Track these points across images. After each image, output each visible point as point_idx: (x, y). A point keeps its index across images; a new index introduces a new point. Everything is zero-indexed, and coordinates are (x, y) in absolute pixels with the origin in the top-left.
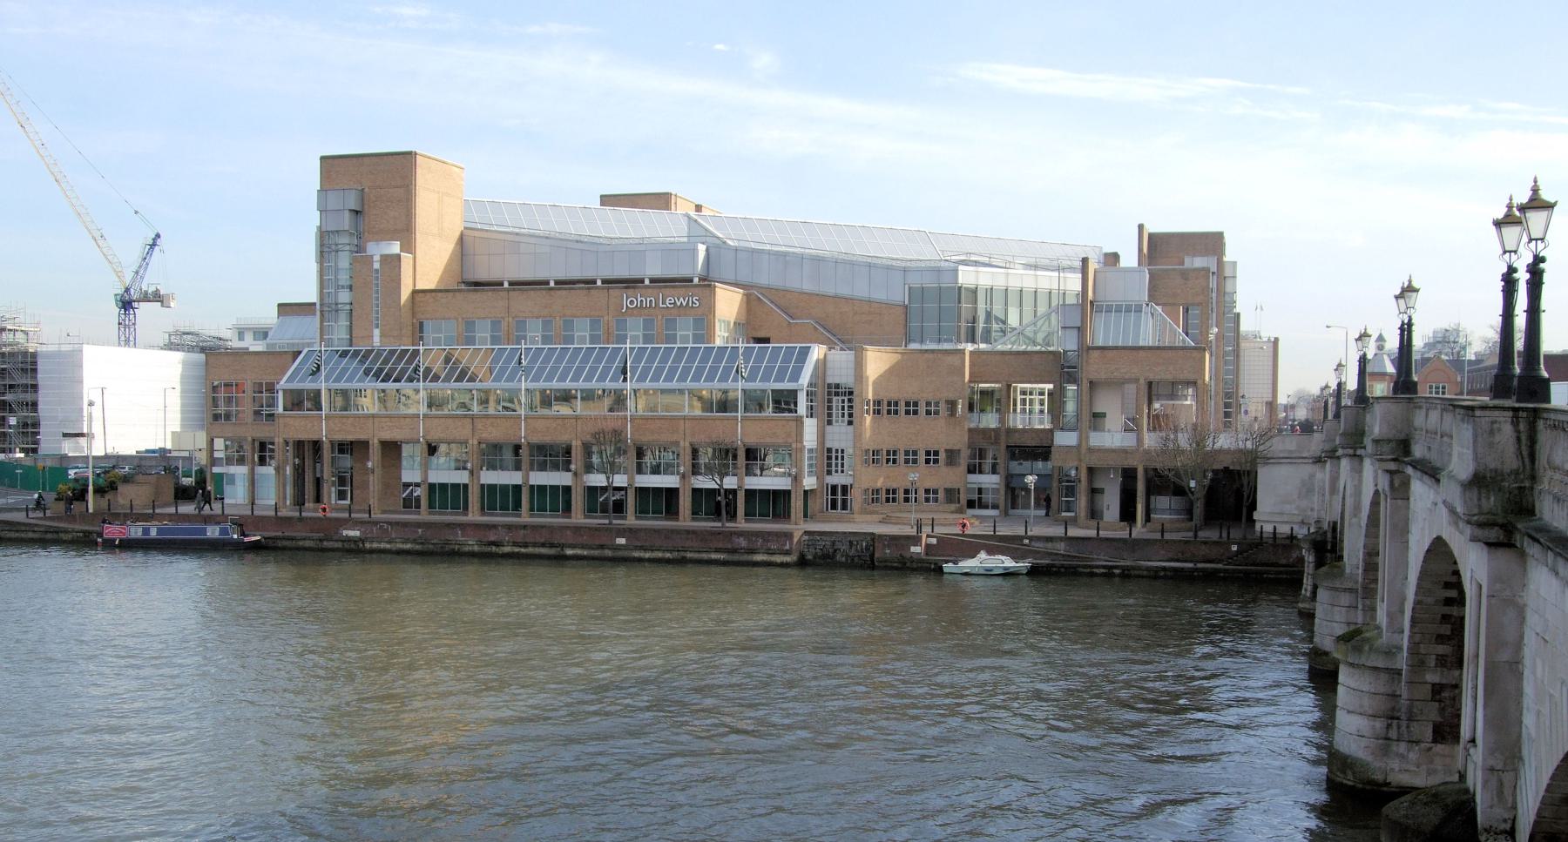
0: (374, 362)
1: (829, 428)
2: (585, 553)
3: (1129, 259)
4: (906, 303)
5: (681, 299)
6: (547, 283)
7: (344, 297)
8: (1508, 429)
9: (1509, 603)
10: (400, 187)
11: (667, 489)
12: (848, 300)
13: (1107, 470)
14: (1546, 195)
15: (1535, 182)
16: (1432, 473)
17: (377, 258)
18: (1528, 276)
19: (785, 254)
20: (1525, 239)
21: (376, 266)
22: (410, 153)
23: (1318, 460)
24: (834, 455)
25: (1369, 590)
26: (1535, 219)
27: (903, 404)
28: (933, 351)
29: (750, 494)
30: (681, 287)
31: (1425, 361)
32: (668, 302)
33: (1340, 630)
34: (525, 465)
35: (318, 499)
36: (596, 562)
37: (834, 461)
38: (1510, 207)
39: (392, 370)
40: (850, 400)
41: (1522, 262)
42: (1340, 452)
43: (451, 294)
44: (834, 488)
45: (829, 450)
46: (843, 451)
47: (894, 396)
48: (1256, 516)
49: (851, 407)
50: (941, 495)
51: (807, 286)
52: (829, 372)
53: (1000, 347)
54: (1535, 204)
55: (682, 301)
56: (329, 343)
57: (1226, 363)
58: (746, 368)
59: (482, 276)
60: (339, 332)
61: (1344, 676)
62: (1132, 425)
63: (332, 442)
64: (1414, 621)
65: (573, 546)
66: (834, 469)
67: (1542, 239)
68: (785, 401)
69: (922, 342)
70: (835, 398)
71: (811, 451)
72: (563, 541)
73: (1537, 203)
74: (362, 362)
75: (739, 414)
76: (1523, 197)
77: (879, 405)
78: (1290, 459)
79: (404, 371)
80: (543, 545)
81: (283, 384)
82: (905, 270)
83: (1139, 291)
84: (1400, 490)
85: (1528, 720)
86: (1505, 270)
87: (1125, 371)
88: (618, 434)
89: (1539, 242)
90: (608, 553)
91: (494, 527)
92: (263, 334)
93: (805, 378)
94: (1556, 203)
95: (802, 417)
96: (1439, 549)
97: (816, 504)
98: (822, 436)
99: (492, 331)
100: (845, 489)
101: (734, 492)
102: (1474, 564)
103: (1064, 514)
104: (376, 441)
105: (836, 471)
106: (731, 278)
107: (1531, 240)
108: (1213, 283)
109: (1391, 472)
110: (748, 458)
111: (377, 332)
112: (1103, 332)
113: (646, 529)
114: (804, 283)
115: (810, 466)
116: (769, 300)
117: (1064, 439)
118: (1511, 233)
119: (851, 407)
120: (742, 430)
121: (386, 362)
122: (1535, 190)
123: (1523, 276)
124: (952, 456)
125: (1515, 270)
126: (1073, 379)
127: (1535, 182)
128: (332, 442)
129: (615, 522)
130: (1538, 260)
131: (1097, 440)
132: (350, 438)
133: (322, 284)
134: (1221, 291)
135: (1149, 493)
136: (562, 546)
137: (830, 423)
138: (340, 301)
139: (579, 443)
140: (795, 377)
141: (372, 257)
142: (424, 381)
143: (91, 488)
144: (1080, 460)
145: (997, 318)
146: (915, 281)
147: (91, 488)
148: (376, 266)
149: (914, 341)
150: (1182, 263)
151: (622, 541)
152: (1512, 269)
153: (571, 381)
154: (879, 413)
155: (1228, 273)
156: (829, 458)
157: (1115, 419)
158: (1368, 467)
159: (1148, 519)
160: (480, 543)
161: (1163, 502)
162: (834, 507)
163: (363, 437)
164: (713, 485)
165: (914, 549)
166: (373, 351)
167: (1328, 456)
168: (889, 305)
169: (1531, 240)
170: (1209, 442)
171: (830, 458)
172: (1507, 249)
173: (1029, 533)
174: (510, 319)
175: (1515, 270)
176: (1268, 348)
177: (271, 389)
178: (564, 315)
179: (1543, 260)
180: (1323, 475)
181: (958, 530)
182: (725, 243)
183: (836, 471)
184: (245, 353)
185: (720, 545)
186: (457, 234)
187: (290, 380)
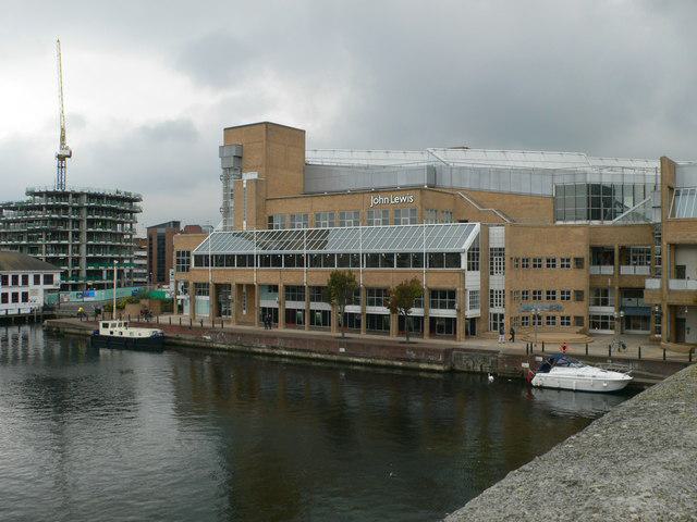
1: (491, 277)
12: (518, 195)
13: (683, 307)
29: (433, 319)
34: (616, 263)
39: (268, 244)
44: (495, 315)
45: (492, 291)
49: (551, 263)
52: (491, 241)
79: (268, 244)
80: (300, 350)
81: (194, 252)
90: (335, 358)
93: (467, 245)
100: (502, 316)
103: (559, 223)
114: (490, 185)
124: (579, 295)
132: (223, 282)
140: (462, 243)
144: (662, 298)
145: (619, 204)
146: (559, 181)
151: (342, 350)
160: (268, 347)
168: (543, 197)
171: (491, 296)
177: (188, 253)
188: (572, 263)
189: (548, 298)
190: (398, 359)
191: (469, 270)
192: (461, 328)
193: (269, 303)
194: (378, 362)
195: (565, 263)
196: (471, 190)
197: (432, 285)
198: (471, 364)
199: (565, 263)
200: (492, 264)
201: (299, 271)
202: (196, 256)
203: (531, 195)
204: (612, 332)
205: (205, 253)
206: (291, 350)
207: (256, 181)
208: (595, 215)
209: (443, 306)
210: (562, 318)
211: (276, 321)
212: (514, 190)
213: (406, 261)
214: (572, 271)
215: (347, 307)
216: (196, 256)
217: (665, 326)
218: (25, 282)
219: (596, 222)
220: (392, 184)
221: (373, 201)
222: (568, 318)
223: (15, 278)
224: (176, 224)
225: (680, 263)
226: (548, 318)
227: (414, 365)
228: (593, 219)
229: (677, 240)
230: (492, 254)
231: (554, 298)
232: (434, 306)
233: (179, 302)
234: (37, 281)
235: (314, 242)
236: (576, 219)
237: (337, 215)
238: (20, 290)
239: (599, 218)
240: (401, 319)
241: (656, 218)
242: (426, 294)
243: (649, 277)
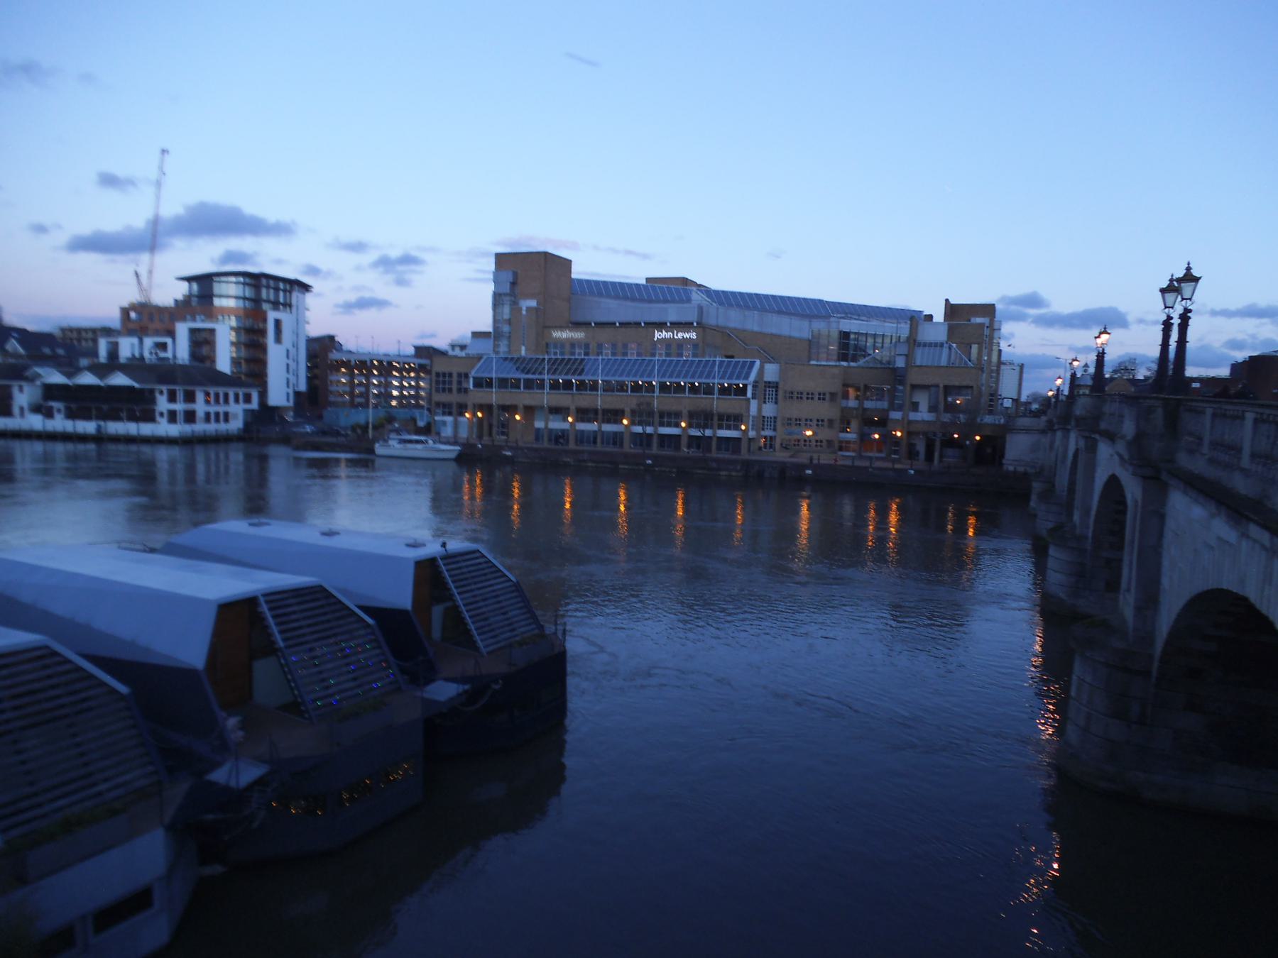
0: (521, 364)
1: (764, 405)
3: (939, 317)
4: (810, 338)
6: (615, 324)
7: (506, 329)
8: (1160, 411)
9: (1156, 515)
12: (779, 336)
13: (917, 434)
14: (1195, 273)
15: (1189, 264)
16: (1111, 437)
17: (524, 308)
18: (1179, 321)
20: (1179, 298)
21: (524, 312)
23: (1043, 432)
25: (1069, 507)
26: (1188, 289)
27: (805, 394)
28: (824, 365)
31: (1112, 379)
32: (679, 335)
33: (1050, 525)
35: (490, 434)
37: (766, 423)
38: (1171, 280)
40: (776, 391)
41: (1179, 309)
42: (1056, 427)
45: (764, 417)
47: (833, 390)
48: (1004, 461)
49: (810, 396)
51: (756, 329)
54: (1187, 278)
56: (497, 353)
57: (992, 377)
59: (581, 319)
60: (503, 348)
61: (1052, 551)
62: (933, 409)
64: (1096, 521)
67: (1190, 299)
69: (818, 360)
70: (768, 389)
71: (753, 417)
73: (1190, 278)
74: (515, 363)
75: (599, 393)
76: (1180, 273)
78: (1027, 430)
79: (537, 369)
81: (473, 373)
83: (941, 336)
84: (1092, 448)
85: (1165, 581)
86: (1165, 318)
89: (1188, 301)
91: (583, 452)
92: (463, 347)
94: (1200, 278)
95: (749, 399)
96: (1113, 484)
98: (760, 409)
101: (710, 438)
102: (1133, 490)
104: (521, 406)
107: (1183, 299)
108: (987, 332)
109: (1086, 438)
110: (719, 420)
111: (523, 348)
112: (921, 357)
115: (753, 425)
116: (735, 336)
118: (1170, 297)
119: (776, 395)
120: (719, 404)
121: (527, 364)
122: (1188, 269)
123: (1176, 321)
124: (831, 422)
125: (1172, 318)
126: (902, 383)
127: (1189, 264)
130: (1187, 311)
131: (913, 416)
133: (495, 321)
134: (991, 338)
135: (1164, 399)
140: (747, 377)
142: (548, 374)
143: (370, 426)
147: (370, 426)
148: (524, 312)
149: (814, 360)
150: (970, 321)
151: (649, 462)
152: (1169, 318)
156: (764, 421)
157: (924, 406)
158: (1073, 436)
159: (941, 461)
161: (950, 452)
163: (514, 403)
164: (699, 434)
167: (1049, 428)
168: (801, 340)
169: (1183, 299)
170: (979, 420)
172: (1167, 306)
173: (873, 466)
175: (1172, 318)
177: (467, 376)
179: (1190, 311)
180: (1045, 440)
181: (832, 462)
184: (456, 357)
188: (827, 397)
191: (753, 399)
195: (822, 397)
196: (735, 329)
197: (722, 410)
199: (822, 397)
200: (765, 395)
202: (474, 378)
203: (790, 337)
207: (536, 310)
214: (826, 404)
218: (226, 401)
219: (845, 364)
220: (662, 320)
223: (217, 395)
228: (843, 360)
230: (765, 386)
232: (662, 424)
234: (237, 400)
237: (620, 345)
238: (221, 409)
239: (846, 361)
241: (900, 363)
242: (716, 418)
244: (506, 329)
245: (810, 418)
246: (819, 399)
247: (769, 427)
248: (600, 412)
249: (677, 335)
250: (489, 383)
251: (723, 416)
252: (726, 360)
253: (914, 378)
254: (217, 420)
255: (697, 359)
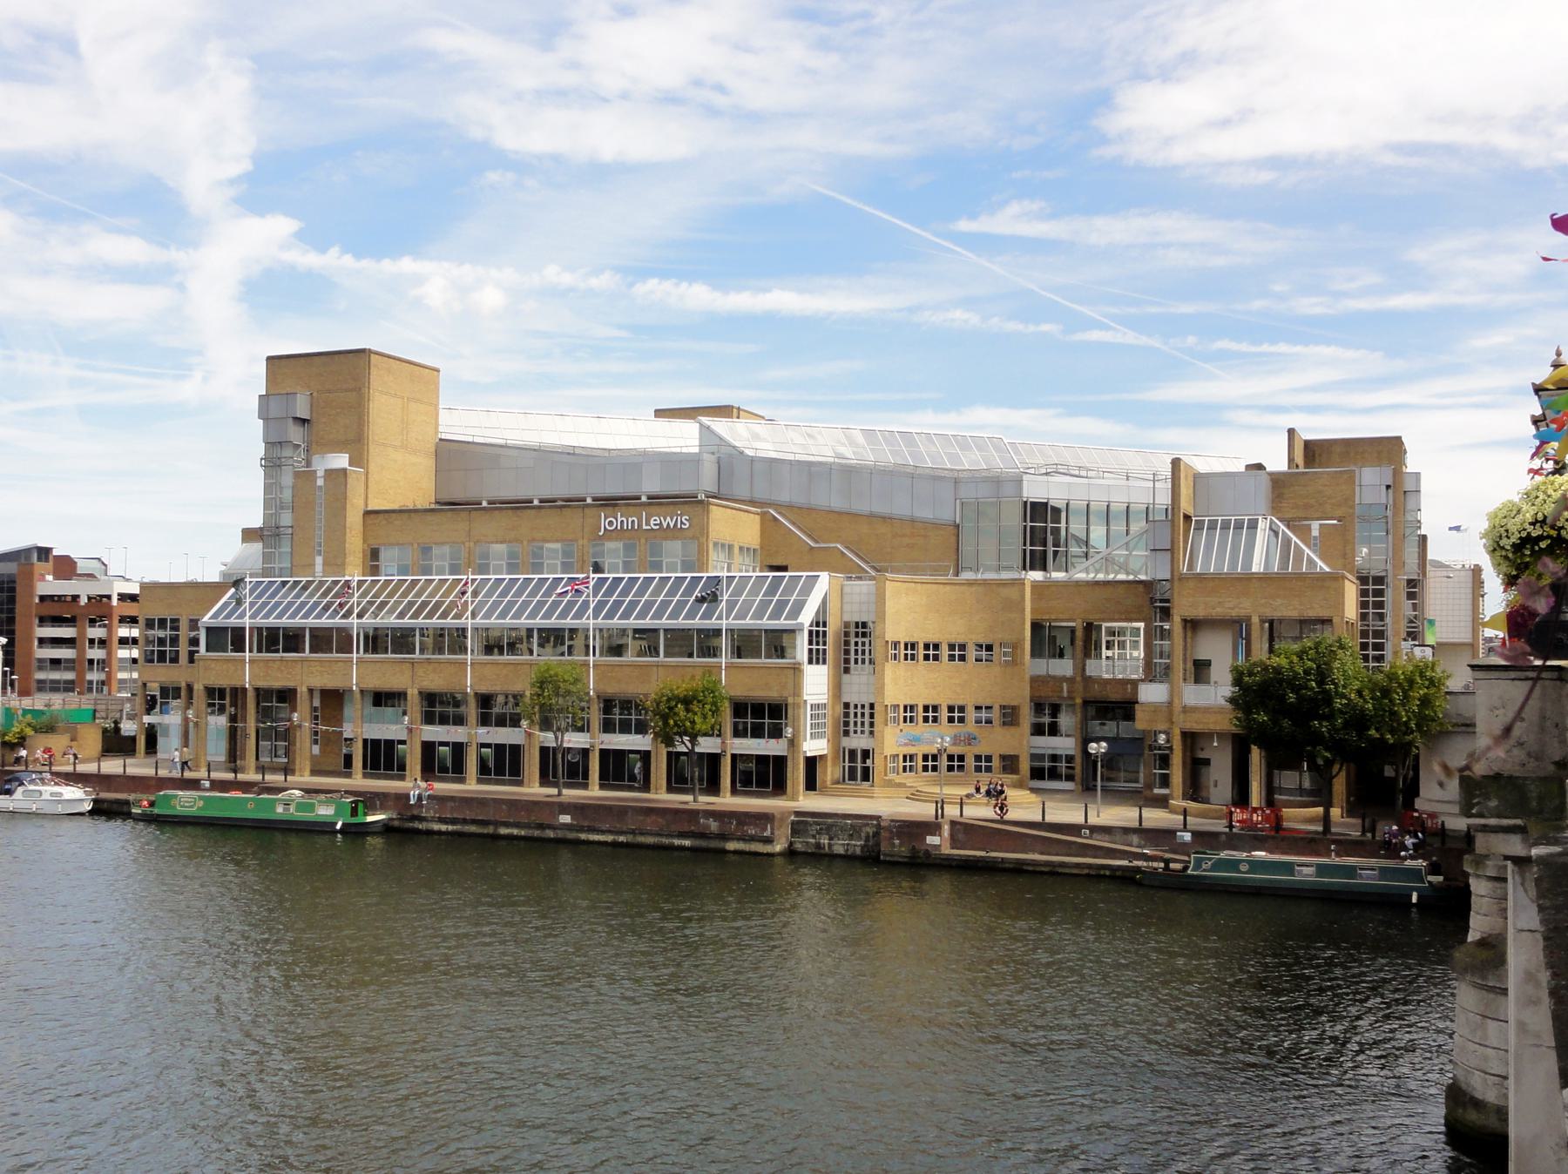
1: (846, 677)
2: (523, 833)
5: (668, 519)
10: (351, 390)
11: (709, 754)
12: (886, 519)
13: (1209, 736)
15: (1559, 354)
17: (320, 473)
19: (810, 464)
21: (320, 482)
22: (363, 351)
24: (852, 711)
30: (668, 504)
32: (652, 522)
36: (189, 829)
37: (852, 719)
43: (406, 515)
44: (853, 753)
45: (847, 705)
46: (872, 706)
47: (932, 638)
50: (996, 763)
53: (1081, 576)
55: (669, 521)
58: (473, 602)
63: (362, 691)
65: (507, 825)
66: (852, 728)
68: (777, 643)
71: (815, 707)
72: (498, 818)
77: (913, 649)
80: (474, 822)
82: (956, 481)
87: (1231, 605)
88: (712, 690)
90: (550, 834)
93: (807, 617)
97: (829, 773)
98: (837, 688)
99: (624, 557)
100: (866, 754)
104: (305, 689)
105: (855, 732)
106: (745, 494)
112: (1209, 556)
113: (495, 800)
117: (1152, 694)
124: (1010, 716)
127: (1559, 354)
128: (257, 690)
129: (565, 791)
136: (497, 824)
137: (847, 671)
138: (282, 524)
139: (416, 692)
141: (315, 471)
145: (1077, 539)
146: (967, 493)
148: (320, 482)
151: (566, 819)
153: (669, 618)
154: (912, 659)
155: (1409, 486)
162: (852, 777)
163: (290, 684)
165: (932, 840)
166: (314, 581)
168: (936, 525)
174: (472, 544)
176: (1467, 578)
178: (534, 540)
182: (742, 453)
183: (855, 732)
185: (686, 829)
186: (433, 450)
187: (215, 616)
189: (951, 720)
190: (682, 835)
191: (810, 662)
192: (797, 774)
193: (387, 728)
194: (641, 839)
196: (790, 507)
198: (825, 841)
201: (234, 660)
204: (1069, 785)
205: (233, 621)
206: (453, 821)
208: (1038, 561)
209: (757, 732)
210: (978, 758)
211: (586, 776)
212: (879, 508)
213: (714, 642)
215: (567, 736)
216: (209, 630)
217: (1177, 774)
219: (1037, 575)
220: (521, 493)
221: (604, 523)
222: (989, 759)
224: (44, 553)
225: (1202, 655)
226: (951, 758)
227: (714, 844)
229: (1199, 612)
231: (961, 720)
233: (29, 716)
235: (265, 604)
236: (999, 569)
240: (673, 758)
242: (472, 703)
243: (1142, 680)
244: (286, 519)
245: (961, 703)
246: (927, 657)
247: (859, 729)
248: (251, 696)
249: (648, 523)
250: (237, 638)
251: (762, 705)
252: (772, 574)
253: (1184, 607)
254: (1073, 768)
255: (690, 575)
